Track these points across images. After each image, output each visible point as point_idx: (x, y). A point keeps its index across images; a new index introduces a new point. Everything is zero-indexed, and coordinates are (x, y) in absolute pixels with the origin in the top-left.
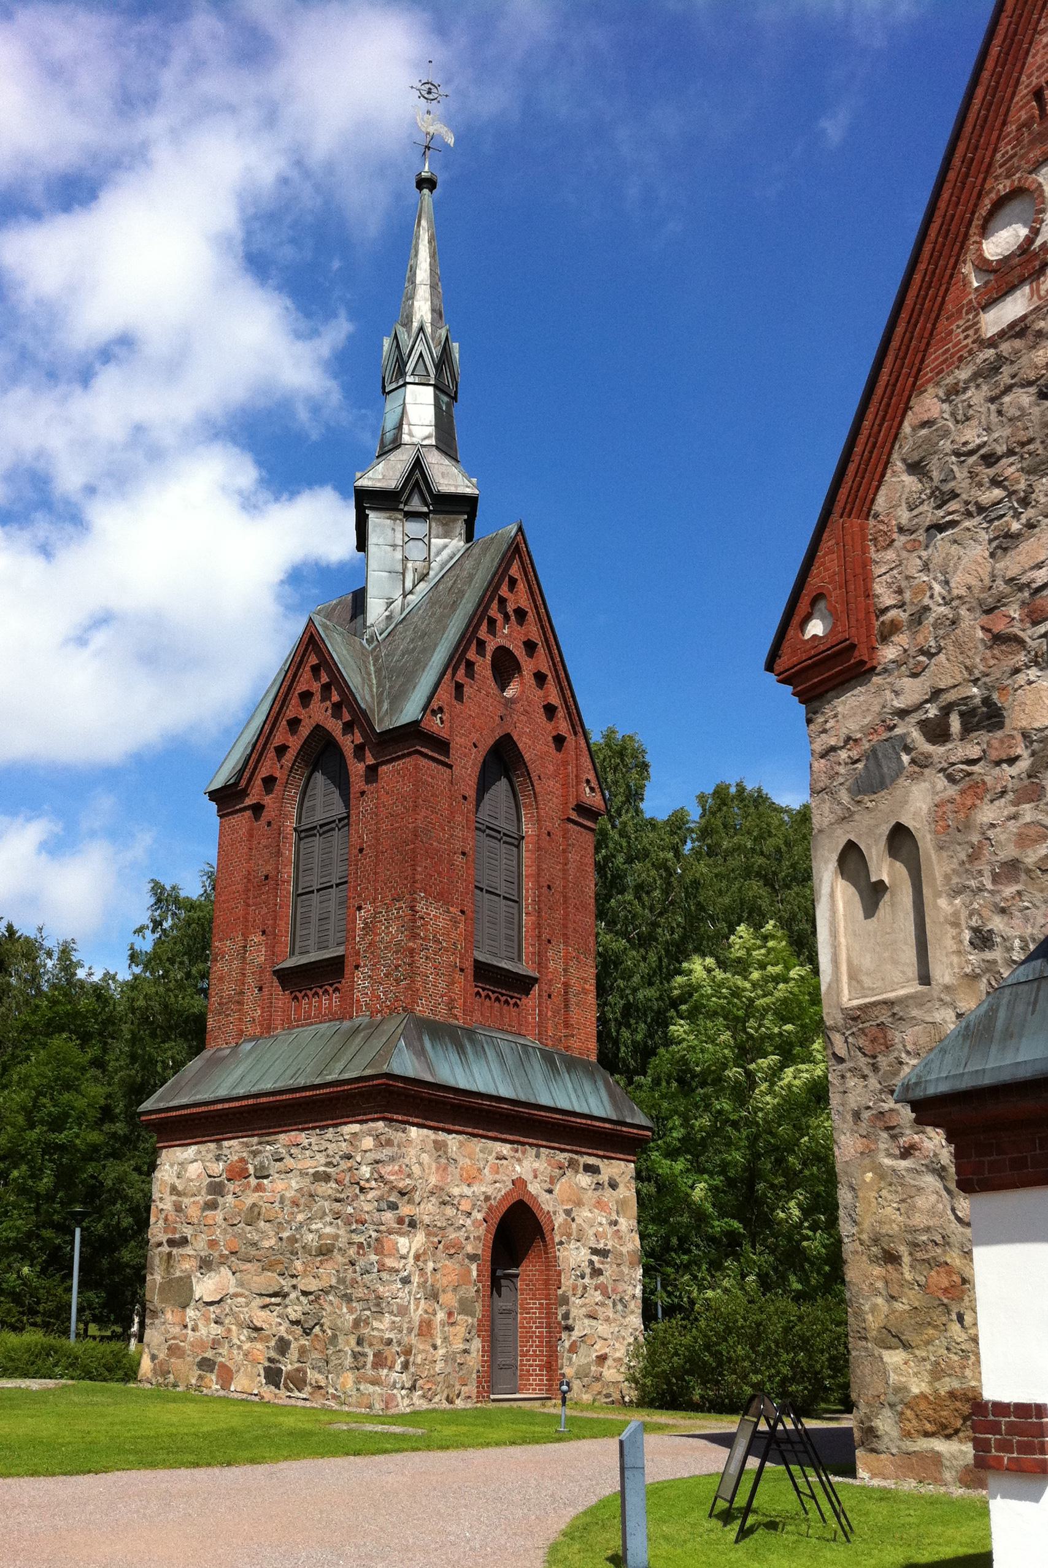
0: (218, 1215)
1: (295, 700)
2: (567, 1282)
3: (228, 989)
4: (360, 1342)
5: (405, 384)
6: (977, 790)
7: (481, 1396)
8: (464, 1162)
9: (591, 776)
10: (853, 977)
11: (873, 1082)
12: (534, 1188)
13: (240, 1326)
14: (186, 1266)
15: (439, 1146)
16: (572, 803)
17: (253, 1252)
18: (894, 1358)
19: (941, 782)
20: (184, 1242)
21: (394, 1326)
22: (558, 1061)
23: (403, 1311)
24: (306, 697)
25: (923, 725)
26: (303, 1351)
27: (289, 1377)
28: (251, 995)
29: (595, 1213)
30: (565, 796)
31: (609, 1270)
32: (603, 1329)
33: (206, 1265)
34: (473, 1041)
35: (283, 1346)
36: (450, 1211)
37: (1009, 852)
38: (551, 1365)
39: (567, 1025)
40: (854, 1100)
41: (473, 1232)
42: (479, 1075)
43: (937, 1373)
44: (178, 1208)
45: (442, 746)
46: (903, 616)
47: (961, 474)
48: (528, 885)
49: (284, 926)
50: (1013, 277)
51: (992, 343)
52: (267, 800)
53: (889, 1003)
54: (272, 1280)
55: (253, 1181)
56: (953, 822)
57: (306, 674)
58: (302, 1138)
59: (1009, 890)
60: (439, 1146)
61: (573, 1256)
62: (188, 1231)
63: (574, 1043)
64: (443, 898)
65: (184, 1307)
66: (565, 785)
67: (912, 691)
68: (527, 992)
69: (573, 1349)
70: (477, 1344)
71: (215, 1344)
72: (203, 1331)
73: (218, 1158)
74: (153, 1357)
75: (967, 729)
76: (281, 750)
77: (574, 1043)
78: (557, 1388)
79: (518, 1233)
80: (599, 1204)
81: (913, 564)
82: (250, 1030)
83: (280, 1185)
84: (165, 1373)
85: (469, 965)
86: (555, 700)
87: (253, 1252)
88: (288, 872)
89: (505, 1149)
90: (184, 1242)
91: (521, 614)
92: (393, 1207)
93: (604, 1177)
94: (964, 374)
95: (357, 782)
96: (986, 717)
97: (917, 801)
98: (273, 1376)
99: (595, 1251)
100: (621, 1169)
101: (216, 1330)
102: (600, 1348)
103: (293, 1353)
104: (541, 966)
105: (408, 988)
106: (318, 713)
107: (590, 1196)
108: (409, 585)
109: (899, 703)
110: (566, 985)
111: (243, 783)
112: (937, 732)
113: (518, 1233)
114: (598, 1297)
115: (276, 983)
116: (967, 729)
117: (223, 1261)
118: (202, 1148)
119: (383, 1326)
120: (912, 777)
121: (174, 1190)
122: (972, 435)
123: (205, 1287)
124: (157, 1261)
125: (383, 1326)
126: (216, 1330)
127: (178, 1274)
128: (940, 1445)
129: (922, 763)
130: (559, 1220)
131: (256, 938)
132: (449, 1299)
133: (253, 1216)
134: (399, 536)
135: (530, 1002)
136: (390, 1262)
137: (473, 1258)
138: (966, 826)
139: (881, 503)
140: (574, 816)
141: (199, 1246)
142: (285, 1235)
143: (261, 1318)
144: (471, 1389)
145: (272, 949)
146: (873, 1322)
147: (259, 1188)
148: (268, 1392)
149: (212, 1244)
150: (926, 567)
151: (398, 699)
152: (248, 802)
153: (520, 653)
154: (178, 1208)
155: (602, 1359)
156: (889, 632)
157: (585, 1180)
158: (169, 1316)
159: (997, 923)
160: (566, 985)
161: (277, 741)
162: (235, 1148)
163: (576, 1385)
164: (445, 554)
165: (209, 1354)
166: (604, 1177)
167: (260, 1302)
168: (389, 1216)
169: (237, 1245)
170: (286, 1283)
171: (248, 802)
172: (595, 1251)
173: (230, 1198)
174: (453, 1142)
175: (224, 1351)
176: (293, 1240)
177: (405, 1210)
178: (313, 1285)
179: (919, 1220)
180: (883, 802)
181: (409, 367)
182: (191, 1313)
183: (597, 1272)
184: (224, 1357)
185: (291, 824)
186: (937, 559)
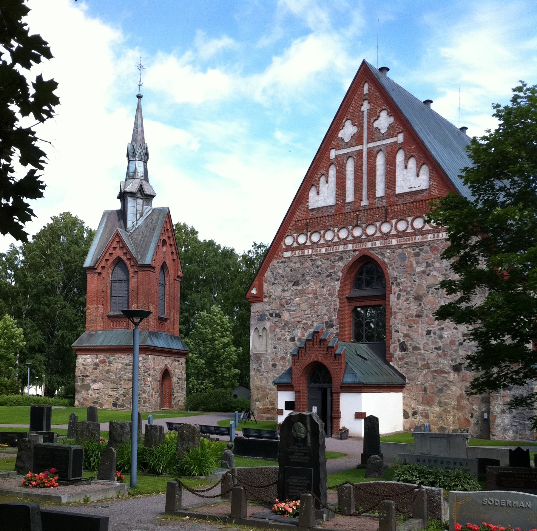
0: (98, 371)
1: (111, 249)
2: (174, 385)
3: (93, 317)
4: (139, 398)
5: (136, 160)
6: (276, 326)
7: (160, 409)
8: (157, 362)
9: (180, 268)
10: (255, 348)
11: (257, 364)
12: (168, 366)
13: (105, 395)
14: (88, 381)
15: (154, 358)
16: (176, 275)
17: (108, 379)
18: (257, 403)
19: (271, 323)
20: (87, 376)
21: (148, 396)
22: (174, 338)
23: (149, 392)
24: (115, 248)
25: (269, 313)
26: (123, 400)
27: (119, 405)
28: (99, 319)
29: (178, 369)
30: (175, 274)
31: (180, 382)
32: (179, 395)
33: (94, 381)
34: (159, 336)
35: (118, 399)
36: (155, 372)
37: (280, 336)
38: (170, 403)
39: (174, 329)
40: (254, 367)
41: (159, 376)
42: (160, 343)
43: (264, 405)
44: (85, 369)
45: (154, 268)
46: (268, 295)
47: (278, 277)
48: (167, 296)
49: (109, 304)
50: (289, 249)
51: (285, 258)
52: (102, 272)
53: (261, 354)
54: (114, 385)
55: (108, 364)
56: (272, 330)
57: (115, 242)
58: (122, 356)
59: (279, 342)
60: (154, 358)
61: (175, 379)
62: (88, 374)
63: (175, 333)
64: (153, 304)
65: (88, 390)
66: (175, 271)
67: (268, 308)
68: (166, 321)
69: (174, 399)
70: (159, 398)
71: (98, 398)
72: (94, 396)
73: (97, 358)
74: (79, 401)
75: (276, 317)
76: (107, 260)
77: (175, 333)
78: (171, 406)
79: (166, 374)
80: (179, 368)
81: (270, 288)
82: (100, 328)
83: (116, 366)
84: (83, 405)
85: (157, 318)
86: (174, 251)
87: (108, 379)
88: (109, 291)
89: (164, 358)
90: (87, 376)
91: (167, 230)
92: (147, 372)
93: (180, 362)
94: (280, 261)
95: (131, 274)
96: (278, 316)
97: (268, 325)
98: (115, 405)
99: (178, 378)
100: (183, 360)
101: (97, 395)
102: (179, 399)
103: (121, 400)
104: (169, 314)
105: (147, 325)
106: (119, 253)
107: (177, 367)
108: (138, 218)
109: (266, 309)
110: (174, 319)
111: (96, 267)
112: (271, 315)
113: (166, 374)
114: (178, 388)
115: (107, 317)
116: (276, 317)
117: (100, 381)
118: (92, 356)
119: (145, 395)
120: (268, 321)
121: (83, 364)
122: (281, 272)
123: (95, 386)
124: (79, 380)
125: (145, 395)
126: (97, 395)
127: (86, 383)
128: (263, 415)
129: (269, 319)
130: (172, 372)
131: (101, 306)
132: (155, 389)
133: (108, 371)
134: (135, 204)
135: (167, 324)
136: (147, 383)
137: (159, 381)
138: (274, 331)
139: (265, 275)
140: (177, 279)
141: (93, 377)
142: (118, 376)
143: (111, 393)
144: (158, 407)
145: (106, 309)
146: (254, 398)
147: (109, 366)
148: (114, 408)
149: (96, 377)
150: (272, 289)
151: (144, 255)
152: (97, 271)
153: (167, 239)
154: (85, 369)
155: (179, 401)
156: (266, 297)
157: (177, 363)
158: (83, 392)
159: (277, 346)
160: (174, 319)
161: (106, 258)
162: (102, 357)
163: (174, 406)
164: (147, 210)
165: (96, 400)
166: (180, 362)
167: (110, 390)
168: (146, 374)
169: (104, 377)
170: (118, 386)
171: (97, 271)
172: (178, 378)
173: (101, 367)
174: (155, 357)
175: (101, 400)
176: (120, 377)
177: (149, 373)
178: (126, 387)
179: (262, 385)
180: (262, 323)
181: (137, 156)
182: (90, 392)
183: (178, 383)
184: (100, 401)
185: (110, 279)
186: (274, 288)
